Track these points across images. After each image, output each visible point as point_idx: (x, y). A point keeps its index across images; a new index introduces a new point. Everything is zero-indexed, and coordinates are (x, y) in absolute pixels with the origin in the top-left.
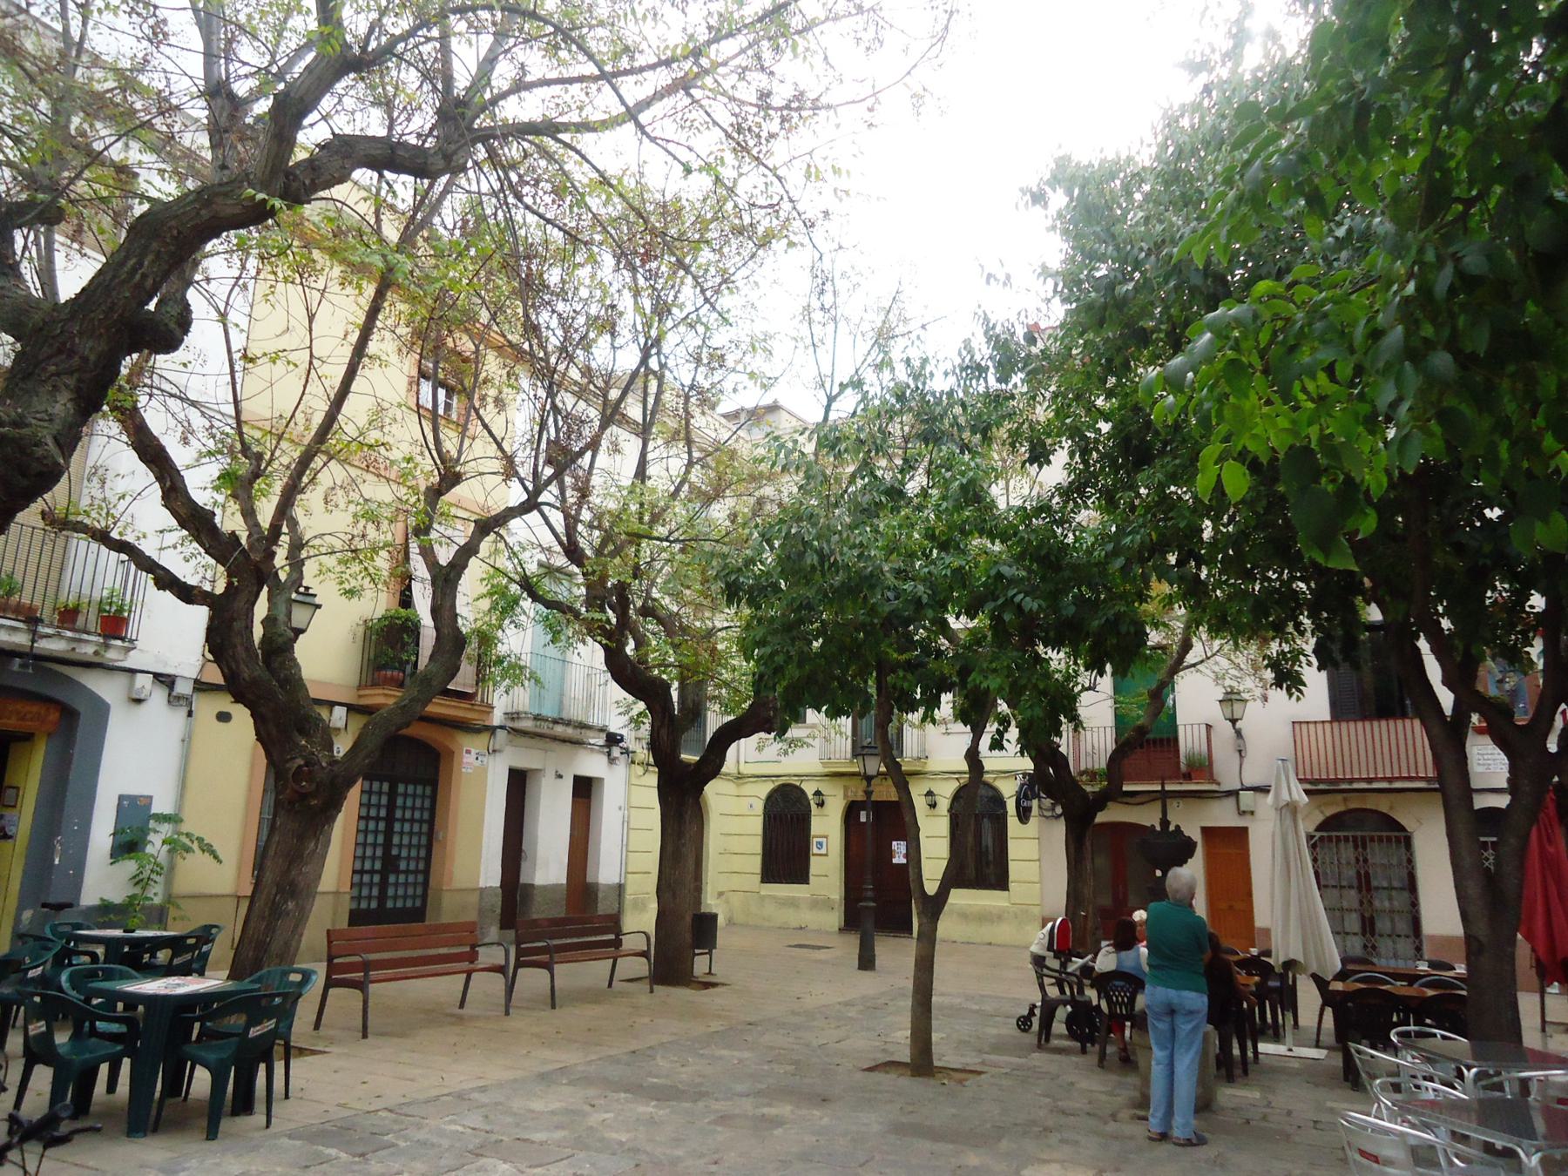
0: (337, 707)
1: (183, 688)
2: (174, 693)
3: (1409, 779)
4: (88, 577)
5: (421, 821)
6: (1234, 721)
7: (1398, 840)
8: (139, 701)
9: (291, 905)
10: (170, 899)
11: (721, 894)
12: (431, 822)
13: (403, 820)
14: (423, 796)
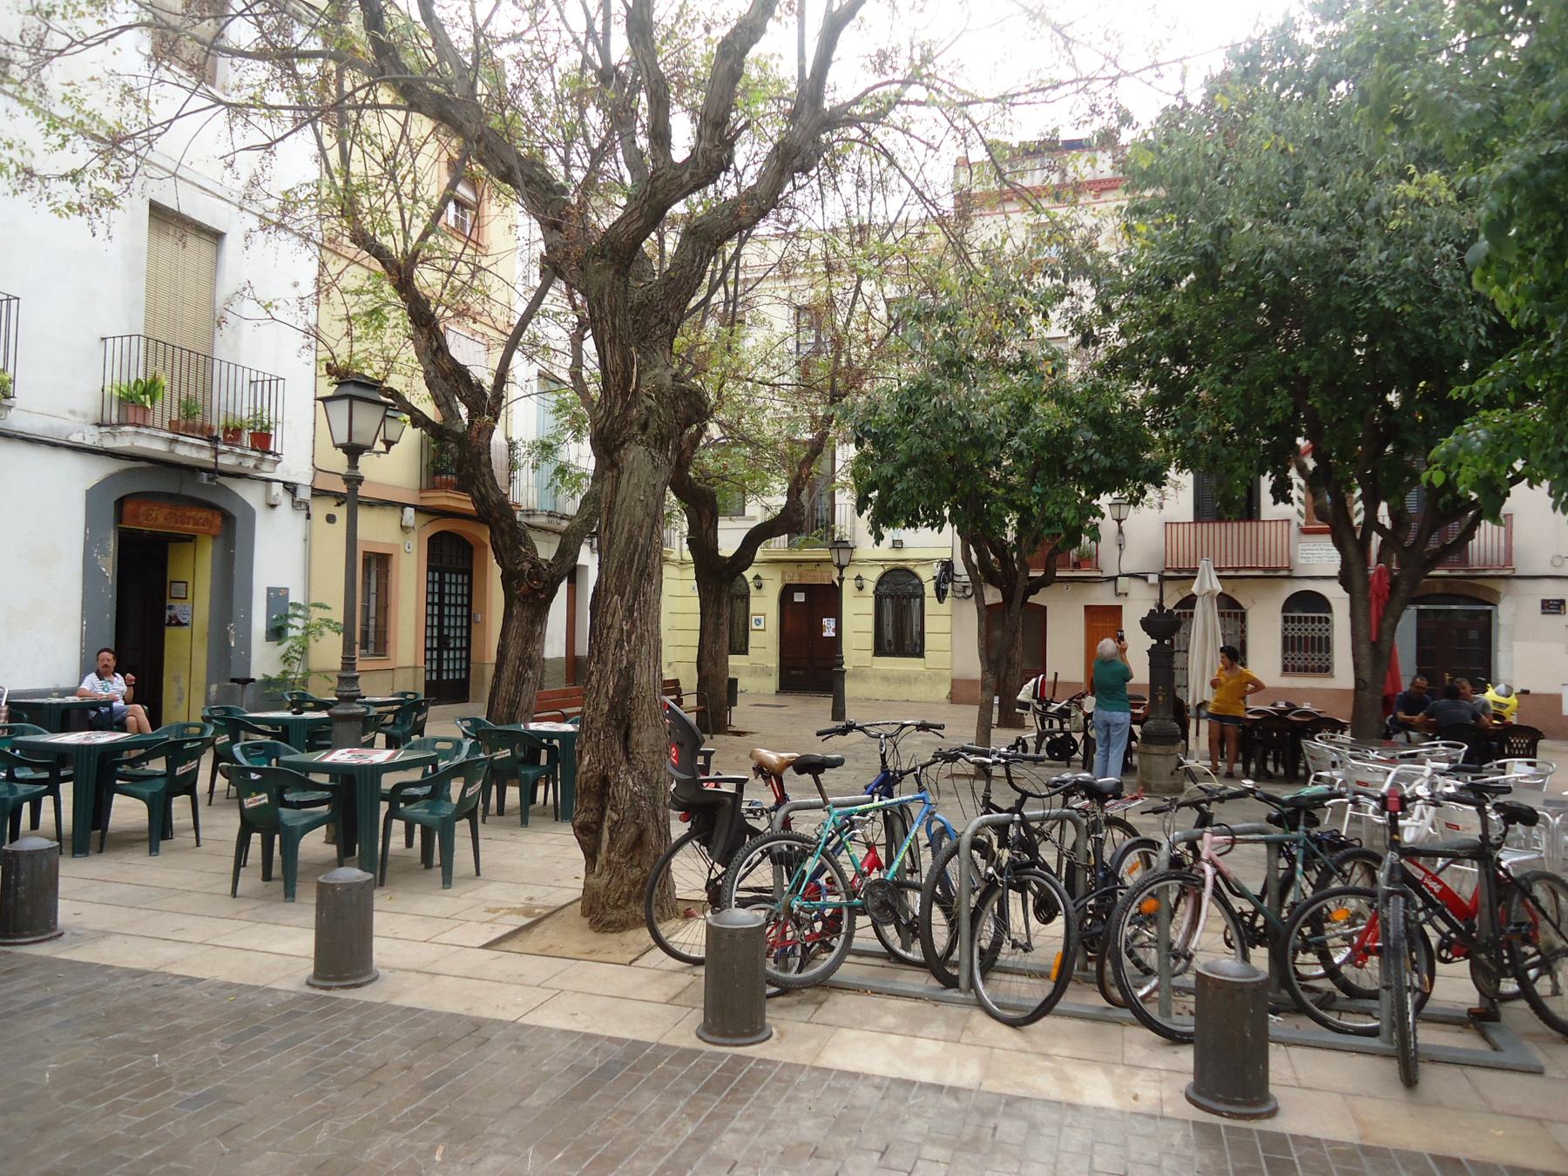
0: (408, 508)
1: (304, 494)
2: (297, 499)
3: (1251, 568)
4: (231, 398)
5: (462, 605)
6: (1119, 521)
8: (273, 506)
9: (530, 673)
10: (308, 672)
11: (670, 664)
13: (450, 605)
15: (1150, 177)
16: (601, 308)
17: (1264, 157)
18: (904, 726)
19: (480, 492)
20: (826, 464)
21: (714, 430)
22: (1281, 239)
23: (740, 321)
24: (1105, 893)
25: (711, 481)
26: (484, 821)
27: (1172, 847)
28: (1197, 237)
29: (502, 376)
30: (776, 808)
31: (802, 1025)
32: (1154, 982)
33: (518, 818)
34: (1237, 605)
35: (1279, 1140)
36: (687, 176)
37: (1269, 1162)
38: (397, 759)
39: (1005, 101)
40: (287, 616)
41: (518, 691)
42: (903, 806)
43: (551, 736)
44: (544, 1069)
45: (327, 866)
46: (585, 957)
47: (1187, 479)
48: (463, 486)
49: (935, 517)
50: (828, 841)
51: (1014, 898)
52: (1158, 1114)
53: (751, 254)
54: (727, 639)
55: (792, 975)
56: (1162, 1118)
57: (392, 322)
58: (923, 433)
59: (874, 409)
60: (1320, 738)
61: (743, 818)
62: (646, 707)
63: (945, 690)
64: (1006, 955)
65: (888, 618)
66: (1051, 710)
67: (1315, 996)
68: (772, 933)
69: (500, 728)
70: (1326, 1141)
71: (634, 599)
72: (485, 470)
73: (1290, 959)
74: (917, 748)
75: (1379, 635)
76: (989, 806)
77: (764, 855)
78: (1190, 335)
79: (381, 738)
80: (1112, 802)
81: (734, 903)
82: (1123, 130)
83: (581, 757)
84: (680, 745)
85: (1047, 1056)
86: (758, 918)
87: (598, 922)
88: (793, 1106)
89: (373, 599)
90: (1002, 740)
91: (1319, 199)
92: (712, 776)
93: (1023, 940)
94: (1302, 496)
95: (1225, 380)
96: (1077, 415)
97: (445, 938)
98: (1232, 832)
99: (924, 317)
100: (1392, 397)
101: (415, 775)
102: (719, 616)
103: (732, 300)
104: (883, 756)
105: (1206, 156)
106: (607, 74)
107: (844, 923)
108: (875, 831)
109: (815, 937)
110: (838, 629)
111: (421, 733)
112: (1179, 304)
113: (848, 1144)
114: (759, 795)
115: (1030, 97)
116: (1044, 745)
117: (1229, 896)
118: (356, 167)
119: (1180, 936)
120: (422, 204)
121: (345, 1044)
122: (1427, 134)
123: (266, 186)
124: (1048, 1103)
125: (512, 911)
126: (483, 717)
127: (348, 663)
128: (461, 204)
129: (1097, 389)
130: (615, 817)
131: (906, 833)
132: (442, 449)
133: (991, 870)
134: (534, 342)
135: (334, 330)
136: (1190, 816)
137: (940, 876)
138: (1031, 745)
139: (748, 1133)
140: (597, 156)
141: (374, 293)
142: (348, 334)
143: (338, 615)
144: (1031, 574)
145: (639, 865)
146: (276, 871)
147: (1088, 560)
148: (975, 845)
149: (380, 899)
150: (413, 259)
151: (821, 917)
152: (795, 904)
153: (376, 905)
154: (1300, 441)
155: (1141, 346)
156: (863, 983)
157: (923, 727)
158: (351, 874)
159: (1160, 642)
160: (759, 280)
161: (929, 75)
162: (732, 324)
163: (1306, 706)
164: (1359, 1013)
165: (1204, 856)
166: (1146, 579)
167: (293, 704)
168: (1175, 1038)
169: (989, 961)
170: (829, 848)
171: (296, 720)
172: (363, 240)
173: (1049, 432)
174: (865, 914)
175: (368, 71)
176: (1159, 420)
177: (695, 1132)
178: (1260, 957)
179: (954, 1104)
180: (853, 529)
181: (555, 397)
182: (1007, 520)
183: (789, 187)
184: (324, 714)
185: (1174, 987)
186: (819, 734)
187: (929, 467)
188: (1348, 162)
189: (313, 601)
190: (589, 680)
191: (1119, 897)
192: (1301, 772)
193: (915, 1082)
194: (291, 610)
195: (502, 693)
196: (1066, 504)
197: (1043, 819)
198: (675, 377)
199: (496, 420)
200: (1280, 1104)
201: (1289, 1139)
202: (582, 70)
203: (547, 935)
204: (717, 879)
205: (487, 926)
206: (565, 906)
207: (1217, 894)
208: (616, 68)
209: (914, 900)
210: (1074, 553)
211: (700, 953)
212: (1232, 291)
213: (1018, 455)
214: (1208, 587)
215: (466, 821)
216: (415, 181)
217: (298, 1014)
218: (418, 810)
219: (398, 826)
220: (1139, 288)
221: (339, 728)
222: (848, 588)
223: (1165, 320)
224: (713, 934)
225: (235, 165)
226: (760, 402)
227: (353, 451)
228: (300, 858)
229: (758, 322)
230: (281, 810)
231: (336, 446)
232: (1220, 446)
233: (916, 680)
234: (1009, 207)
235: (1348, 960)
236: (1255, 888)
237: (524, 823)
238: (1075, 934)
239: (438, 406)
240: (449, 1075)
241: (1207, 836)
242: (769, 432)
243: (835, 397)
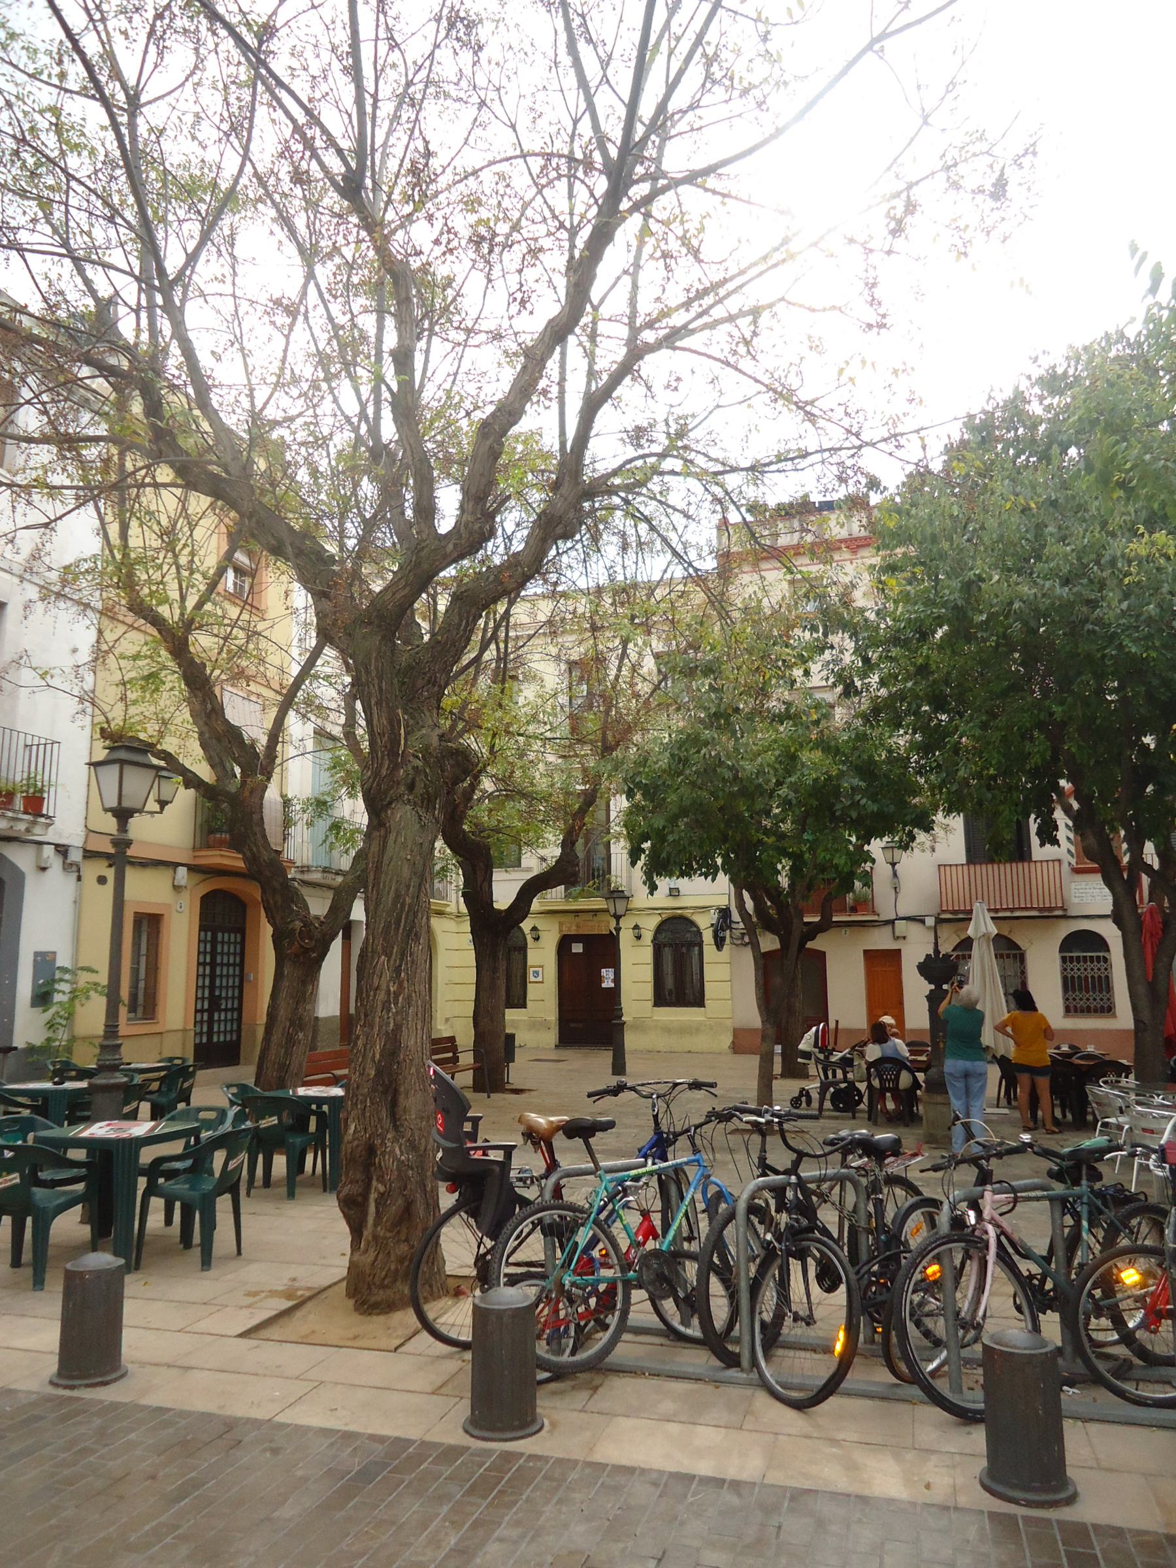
1: (76, 856)
3: (1026, 909)
5: (234, 965)
6: (893, 864)
7: (1015, 956)
8: (44, 869)
9: (301, 1035)
10: (73, 1039)
11: (447, 1020)
12: (242, 965)
13: (222, 965)
14: (235, 943)
15: (901, 536)
16: (368, 672)
17: (1005, 516)
18: (676, 1085)
19: (251, 850)
20: (601, 815)
21: (487, 785)
22: (1026, 590)
23: (512, 677)
24: (888, 1258)
25: (485, 834)
26: (248, 1194)
27: (953, 1207)
28: (947, 592)
29: (276, 732)
30: (546, 1176)
31: (576, 1414)
32: (944, 1354)
33: (284, 1190)
34: (1016, 947)
35: (1078, 1533)
36: (450, 546)
37: (1069, 1555)
38: (156, 1132)
39: (756, 470)
40: (54, 981)
41: (289, 1054)
42: (678, 1170)
43: (320, 1101)
44: (300, 1473)
45: (78, 1250)
46: (349, 1343)
47: (957, 822)
48: (237, 844)
49: (708, 866)
50: (601, 1210)
51: (795, 1266)
52: (951, 1504)
53: (520, 613)
54: (503, 993)
55: (566, 1358)
56: (956, 1508)
57: (168, 686)
58: (693, 784)
59: (643, 761)
60: (1105, 1082)
61: (511, 1187)
62: (413, 1070)
63: (727, 1040)
64: (790, 1330)
65: (668, 968)
66: (833, 1059)
67: (1111, 1364)
68: (544, 1311)
69: (267, 1094)
70: (1130, 1530)
71: (401, 960)
72: (256, 829)
73: (1081, 1325)
74: (693, 1107)
75: (1155, 976)
76: (765, 1168)
77: (534, 1225)
78: (947, 683)
79: (145, 1107)
80: (891, 1159)
81: (503, 1280)
82: (872, 494)
83: (347, 1126)
84: (445, 1111)
85: (834, 1442)
86: (526, 1297)
87: (364, 1303)
88: (564, 1509)
89: (143, 960)
90: (785, 1089)
91: (1060, 554)
92: (480, 1143)
93: (803, 1312)
94: (1071, 836)
95: (984, 726)
96: (844, 763)
97: (202, 1326)
98: (1013, 1190)
99: (690, 672)
100: (1148, 740)
101: (176, 1148)
102: (495, 970)
103: (502, 658)
104: (656, 1117)
105: (951, 516)
106: (378, 452)
107: (619, 1298)
108: (650, 1197)
109: (589, 1313)
110: (617, 979)
111: (187, 1101)
112: (935, 655)
113: (623, 1550)
114: (528, 1161)
115: (781, 466)
116: (828, 1096)
117: (1016, 1258)
118: (134, 542)
119: (966, 1305)
120: (197, 576)
121: (86, 1451)
122: (1150, 498)
123: (47, 560)
124: (834, 1496)
125: (273, 1293)
126: (251, 1082)
127: (111, 1029)
128: (239, 571)
129: (861, 737)
130: (381, 1188)
131: (682, 1198)
132: (217, 807)
133: (769, 1237)
134: (308, 702)
135: (109, 695)
136: (968, 1174)
137: (718, 1243)
138: (815, 1096)
139: (515, 1542)
140: (369, 526)
141: (151, 657)
142: (123, 698)
143: (103, 978)
144: (806, 920)
145: (407, 1240)
146: (27, 1256)
147: (865, 904)
148: (752, 1209)
149: (132, 1285)
150: (189, 625)
151: (595, 1292)
152: (567, 1280)
153: (127, 1292)
154: (1063, 783)
155: (901, 696)
156: (640, 1364)
157: (696, 1085)
158: (103, 1260)
159: (939, 986)
160: (530, 637)
161: (686, 448)
162: (503, 681)
163: (1090, 1049)
164: (1157, 1382)
165: (986, 1214)
166: (923, 922)
167: (56, 1073)
168: (965, 1416)
169: (772, 1336)
170: (603, 1216)
171: (56, 1091)
172: (143, 611)
173: (816, 780)
174: (641, 1287)
175: (147, 454)
176: (924, 767)
177: (457, 1544)
178: (1051, 1322)
179: (735, 1500)
180: (630, 878)
181: (329, 755)
182: (779, 867)
183: (553, 552)
184: (83, 1084)
185: (964, 1359)
186: (590, 1095)
187: (700, 817)
188: (1085, 521)
189: (81, 965)
190: (356, 1044)
191: (903, 1261)
192: (1090, 1118)
193: (694, 1477)
194: (58, 975)
195: (272, 1055)
196: (837, 850)
197: (821, 1180)
198: (441, 737)
199: (269, 779)
200: (1079, 1489)
201: (1090, 1528)
202: (355, 447)
203: (309, 1320)
204: (485, 1254)
205: (245, 1312)
206: (330, 1286)
207: (1003, 1257)
208: (386, 446)
209: (691, 1270)
210: (850, 897)
211: (466, 1336)
212: (985, 640)
213: (786, 803)
214: (983, 930)
215: (228, 1196)
216: (193, 554)
217: (39, 1418)
218: (179, 1186)
219: (157, 1203)
220: (896, 640)
221: (99, 1099)
222: (626, 938)
223: (923, 670)
224: (481, 1316)
225: (17, 541)
226: (532, 756)
227: (123, 814)
228: (51, 1241)
229: (532, 677)
230: (35, 1189)
231: (106, 810)
232: (984, 790)
233: (698, 1030)
234: (764, 565)
235: (1142, 1325)
236: (1042, 1248)
237: (291, 1195)
238: (856, 1304)
239: (212, 766)
240: (196, 1484)
241: (988, 1195)
242: (542, 784)
243: (607, 749)
